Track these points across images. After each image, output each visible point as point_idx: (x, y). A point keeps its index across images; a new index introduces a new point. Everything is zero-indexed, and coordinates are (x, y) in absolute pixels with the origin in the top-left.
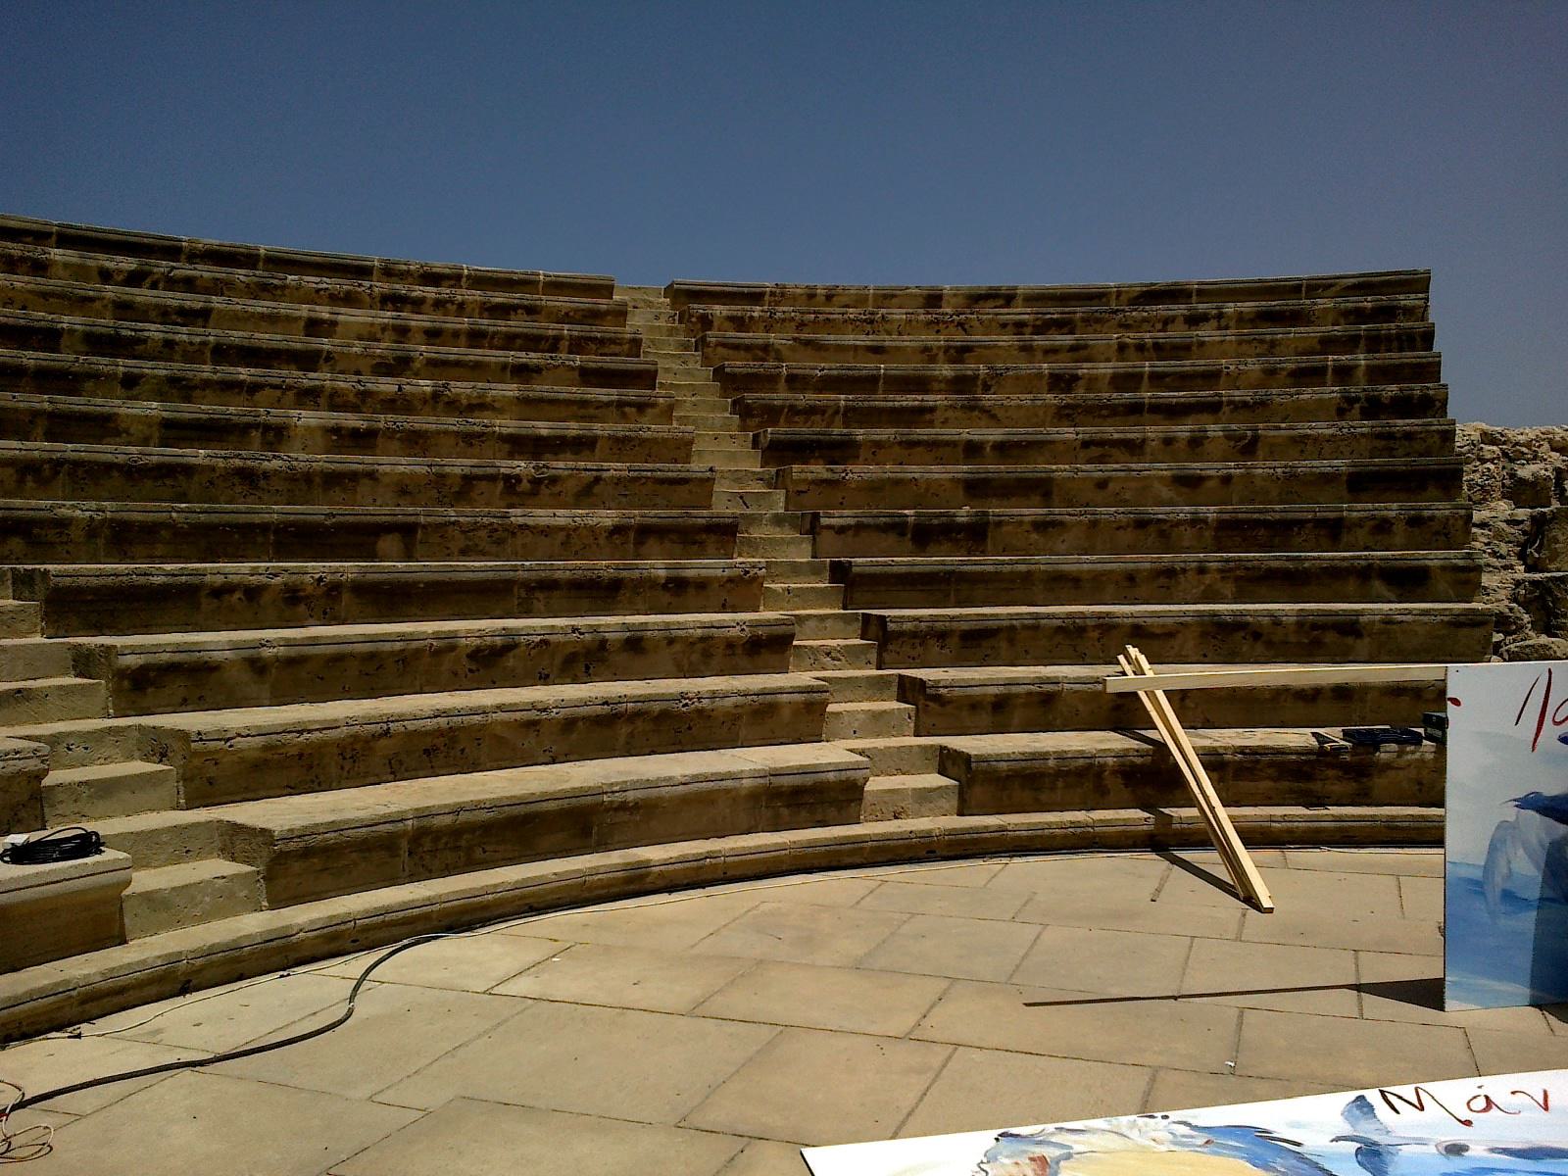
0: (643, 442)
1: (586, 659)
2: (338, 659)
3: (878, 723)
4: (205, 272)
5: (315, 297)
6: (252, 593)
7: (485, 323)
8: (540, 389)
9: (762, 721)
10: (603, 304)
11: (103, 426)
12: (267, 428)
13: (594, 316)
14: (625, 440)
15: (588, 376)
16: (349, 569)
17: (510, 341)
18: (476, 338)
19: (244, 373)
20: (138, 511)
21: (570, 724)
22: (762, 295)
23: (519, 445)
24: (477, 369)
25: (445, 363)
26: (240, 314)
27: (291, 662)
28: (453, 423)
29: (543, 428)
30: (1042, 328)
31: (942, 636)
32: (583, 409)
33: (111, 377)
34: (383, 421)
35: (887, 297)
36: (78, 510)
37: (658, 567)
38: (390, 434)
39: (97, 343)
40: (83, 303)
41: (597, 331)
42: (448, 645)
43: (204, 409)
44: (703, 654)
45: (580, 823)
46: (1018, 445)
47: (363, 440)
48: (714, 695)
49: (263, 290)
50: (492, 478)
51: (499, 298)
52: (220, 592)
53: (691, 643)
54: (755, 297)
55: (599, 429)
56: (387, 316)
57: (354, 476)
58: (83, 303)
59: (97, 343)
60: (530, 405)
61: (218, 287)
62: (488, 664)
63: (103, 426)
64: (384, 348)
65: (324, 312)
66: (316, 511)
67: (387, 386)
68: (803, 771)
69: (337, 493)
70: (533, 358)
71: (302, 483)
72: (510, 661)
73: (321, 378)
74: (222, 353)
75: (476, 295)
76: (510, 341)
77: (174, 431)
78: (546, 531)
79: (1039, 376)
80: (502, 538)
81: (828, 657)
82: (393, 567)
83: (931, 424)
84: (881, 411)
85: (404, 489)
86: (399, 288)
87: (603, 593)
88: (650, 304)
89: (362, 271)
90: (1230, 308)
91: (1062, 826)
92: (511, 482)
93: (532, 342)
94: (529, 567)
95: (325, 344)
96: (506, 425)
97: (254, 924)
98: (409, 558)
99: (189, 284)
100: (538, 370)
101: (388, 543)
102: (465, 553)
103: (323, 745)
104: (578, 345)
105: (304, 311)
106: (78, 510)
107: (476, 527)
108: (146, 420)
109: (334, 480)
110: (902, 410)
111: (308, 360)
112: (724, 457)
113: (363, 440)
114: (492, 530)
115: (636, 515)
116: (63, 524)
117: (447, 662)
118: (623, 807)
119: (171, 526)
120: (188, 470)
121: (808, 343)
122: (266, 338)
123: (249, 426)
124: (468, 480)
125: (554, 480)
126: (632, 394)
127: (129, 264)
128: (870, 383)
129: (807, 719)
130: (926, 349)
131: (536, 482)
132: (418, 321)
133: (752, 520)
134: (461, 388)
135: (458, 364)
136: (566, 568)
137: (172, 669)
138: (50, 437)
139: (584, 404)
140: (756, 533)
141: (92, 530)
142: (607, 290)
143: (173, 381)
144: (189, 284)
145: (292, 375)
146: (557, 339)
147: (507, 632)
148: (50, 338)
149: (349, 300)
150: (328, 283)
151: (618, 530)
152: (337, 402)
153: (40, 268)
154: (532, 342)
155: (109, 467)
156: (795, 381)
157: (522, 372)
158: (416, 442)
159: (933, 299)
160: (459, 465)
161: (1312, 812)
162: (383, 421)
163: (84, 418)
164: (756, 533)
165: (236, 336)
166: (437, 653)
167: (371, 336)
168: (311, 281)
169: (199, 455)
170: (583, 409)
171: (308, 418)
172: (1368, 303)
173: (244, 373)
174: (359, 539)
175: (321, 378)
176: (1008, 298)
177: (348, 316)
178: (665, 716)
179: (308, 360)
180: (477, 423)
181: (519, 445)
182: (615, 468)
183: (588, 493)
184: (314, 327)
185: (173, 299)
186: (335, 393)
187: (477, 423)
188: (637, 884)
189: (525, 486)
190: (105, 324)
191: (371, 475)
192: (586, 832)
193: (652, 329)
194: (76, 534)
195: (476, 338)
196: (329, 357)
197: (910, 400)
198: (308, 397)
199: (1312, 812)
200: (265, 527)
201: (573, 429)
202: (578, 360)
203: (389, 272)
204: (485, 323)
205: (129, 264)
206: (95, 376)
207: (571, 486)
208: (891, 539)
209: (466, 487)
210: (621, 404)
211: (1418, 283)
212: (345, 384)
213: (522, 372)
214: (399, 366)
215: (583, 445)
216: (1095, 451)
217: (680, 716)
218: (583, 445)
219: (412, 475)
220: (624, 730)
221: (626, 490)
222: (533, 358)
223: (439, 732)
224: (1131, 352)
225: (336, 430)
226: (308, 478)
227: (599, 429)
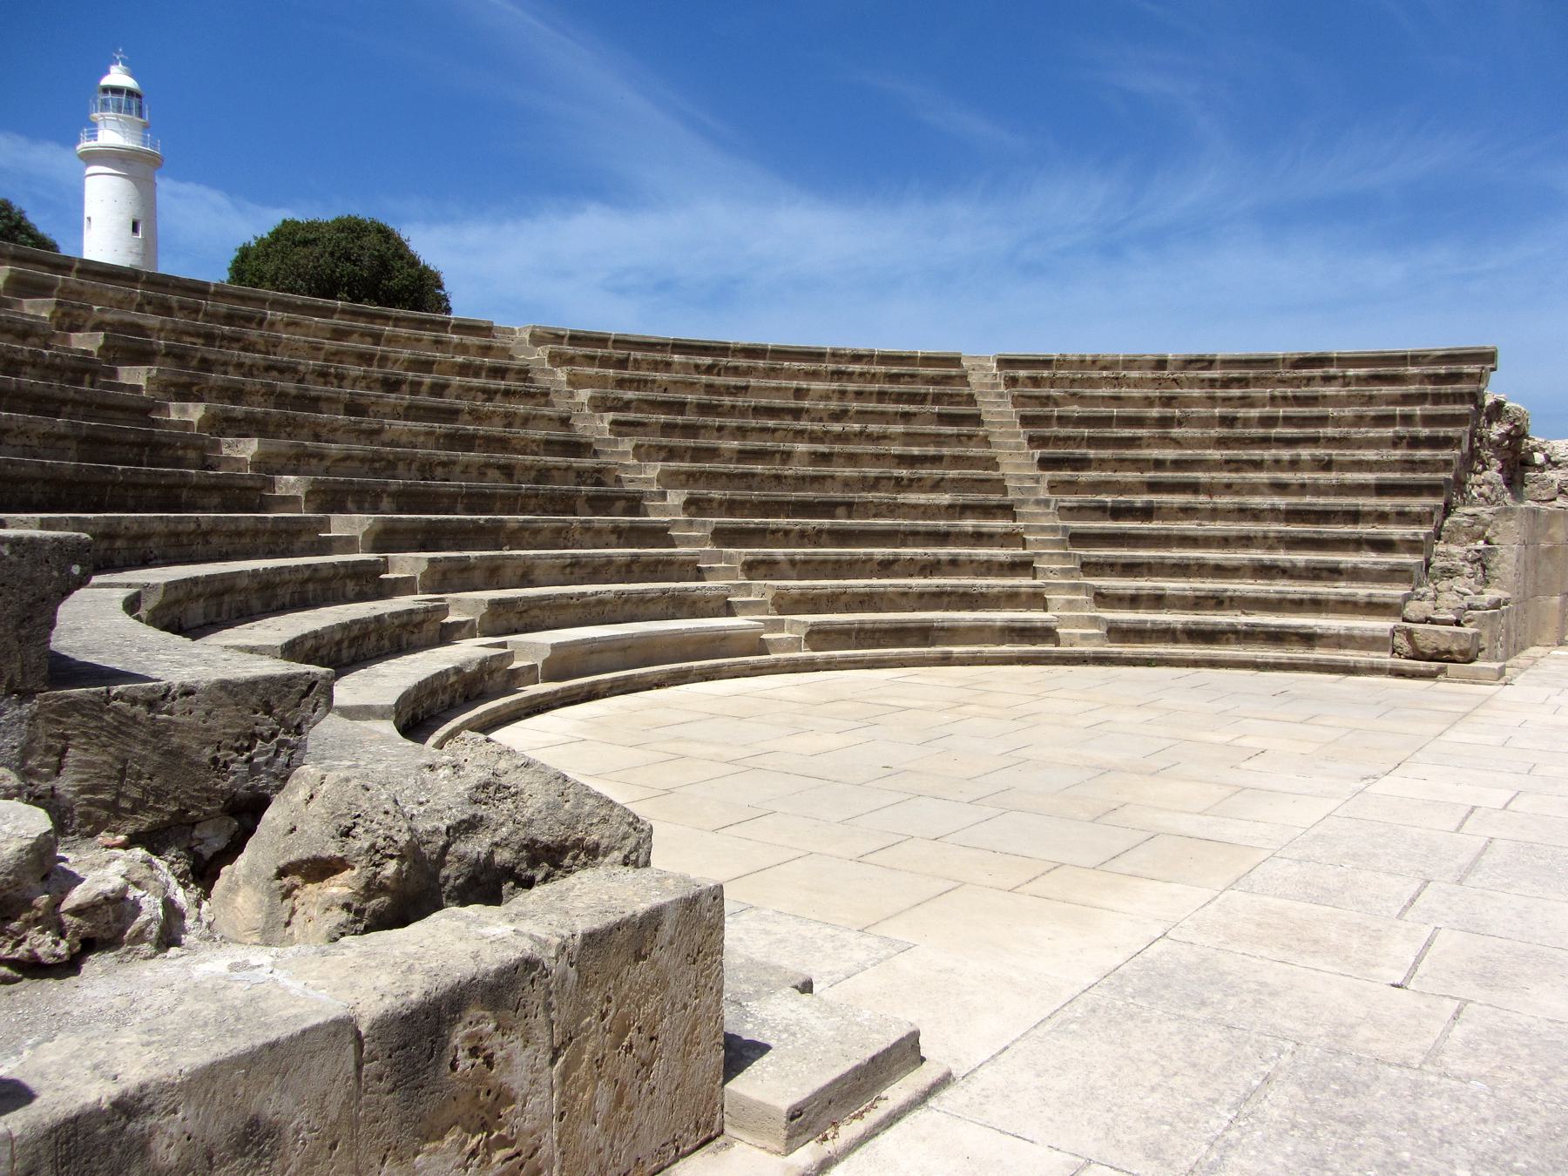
0: (968, 458)
1: (930, 568)
2: (824, 562)
3: (1071, 604)
4: (743, 362)
5: (794, 375)
6: (787, 533)
7: (887, 387)
8: (916, 428)
9: (1011, 599)
10: (954, 371)
11: (713, 453)
12: (783, 452)
13: (946, 379)
14: (959, 457)
15: (943, 419)
16: (826, 522)
17: (900, 398)
18: (882, 396)
19: (771, 423)
20: (740, 495)
21: (921, 595)
22: (1050, 361)
23: (904, 460)
24: (882, 416)
25: (866, 412)
26: (765, 389)
27: (805, 562)
28: (871, 449)
29: (916, 451)
30: (1227, 383)
31: (1112, 565)
32: (938, 439)
33: (712, 427)
34: (837, 448)
35: (1130, 363)
36: (716, 494)
37: (968, 524)
38: (839, 455)
39: (704, 409)
40: (691, 386)
41: (948, 389)
42: (869, 559)
43: (752, 444)
44: (989, 567)
45: (925, 634)
46: (1186, 461)
47: (825, 458)
48: (988, 586)
49: (772, 372)
50: (889, 478)
51: (895, 370)
52: (774, 532)
53: (982, 563)
54: (1046, 363)
55: (946, 451)
56: (835, 386)
57: (824, 478)
58: (691, 386)
59: (704, 409)
60: (910, 438)
61: (748, 372)
62: (886, 567)
63: (713, 453)
64: (834, 405)
65: (804, 385)
66: (809, 495)
67: (837, 427)
68: (1025, 621)
69: (816, 486)
70: (912, 408)
71: (802, 481)
72: (895, 567)
73: (804, 424)
74: (758, 411)
75: (882, 369)
76: (900, 398)
77: (744, 455)
78: (915, 506)
79: (1213, 418)
80: (893, 509)
81: (1054, 569)
82: (844, 522)
83: (1140, 447)
84: (1110, 439)
85: (847, 484)
86: (838, 365)
87: (942, 538)
88: (982, 367)
89: (818, 356)
90: (1351, 372)
91: (890, 622)
92: (899, 480)
93: (912, 398)
94: (904, 523)
95: (806, 404)
96: (896, 449)
97: (805, 654)
98: (849, 517)
99: (736, 371)
100: (915, 414)
101: (840, 511)
102: (875, 516)
103: (820, 596)
104: (937, 398)
105: (794, 384)
106: (716, 494)
107: (881, 504)
108: (731, 450)
109: (815, 479)
110: (1122, 439)
111: (797, 413)
112: (1017, 463)
113: (825, 458)
114: (889, 505)
115: (961, 499)
116: (710, 500)
117: (868, 566)
118: (942, 629)
119: (751, 502)
120: (753, 475)
121: (1074, 395)
122: (778, 402)
123: (775, 452)
124: (878, 479)
125: (920, 479)
126: (965, 430)
127: (708, 360)
128: (1106, 421)
129: (1037, 600)
130: (1147, 398)
131: (911, 480)
132: (852, 387)
133: (1023, 502)
134: (873, 428)
135: (872, 412)
136: (922, 524)
137: (763, 562)
138: (693, 460)
139: (939, 435)
140: (1024, 510)
141: (721, 503)
142: (954, 361)
143: (739, 428)
144: (736, 371)
145: (788, 423)
146: (926, 395)
147: (896, 554)
148: (680, 407)
149: (814, 375)
150: (804, 366)
151: (951, 506)
152: (813, 437)
153: (668, 365)
154: (912, 398)
155: (722, 474)
156: (1063, 420)
157: (906, 417)
158: (852, 459)
159: (1161, 364)
160: (873, 472)
161: (1098, 498)
162: (837, 448)
163: (707, 450)
164: (1024, 510)
165: (764, 402)
166: (864, 562)
167: (826, 396)
168: (796, 365)
169: (759, 468)
170: (938, 439)
171: (802, 447)
172: (1442, 370)
173: (771, 423)
174: (828, 509)
175: (804, 424)
176: (1209, 363)
177: (817, 386)
178: (965, 594)
179: (797, 413)
180: (881, 448)
181: (904, 460)
182: (953, 473)
183: (937, 486)
184: (799, 393)
185: (733, 381)
186: (812, 432)
187: (881, 448)
188: (946, 660)
189: (905, 482)
190: (705, 398)
191: (832, 477)
192: (926, 638)
193: (982, 385)
194: (715, 505)
195: (882, 396)
196: (808, 411)
197: (1127, 432)
198: (799, 434)
199: (1098, 498)
200: (789, 503)
201: (931, 450)
202: (937, 409)
203: (836, 355)
204: (887, 387)
205: (708, 360)
206: (705, 427)
207: (929, 483)
208: (1099, 514)
209: (875, 484)
210: (959, 436)
211: (1487, 357)
212: (817, 427)
213: (906, 417)
214: (838, 416)
215: (936, 460)
216: (1233, 466)
217: (971, 595)
218: (936, 460)
219: (851, 478)
220: (946, 600)
221: (958, 485)
222: (912, 408)
223: (866, 594)
224: (1279, 401)
225: (815, 453)
226: (803, 478)
227: (946, 451)
